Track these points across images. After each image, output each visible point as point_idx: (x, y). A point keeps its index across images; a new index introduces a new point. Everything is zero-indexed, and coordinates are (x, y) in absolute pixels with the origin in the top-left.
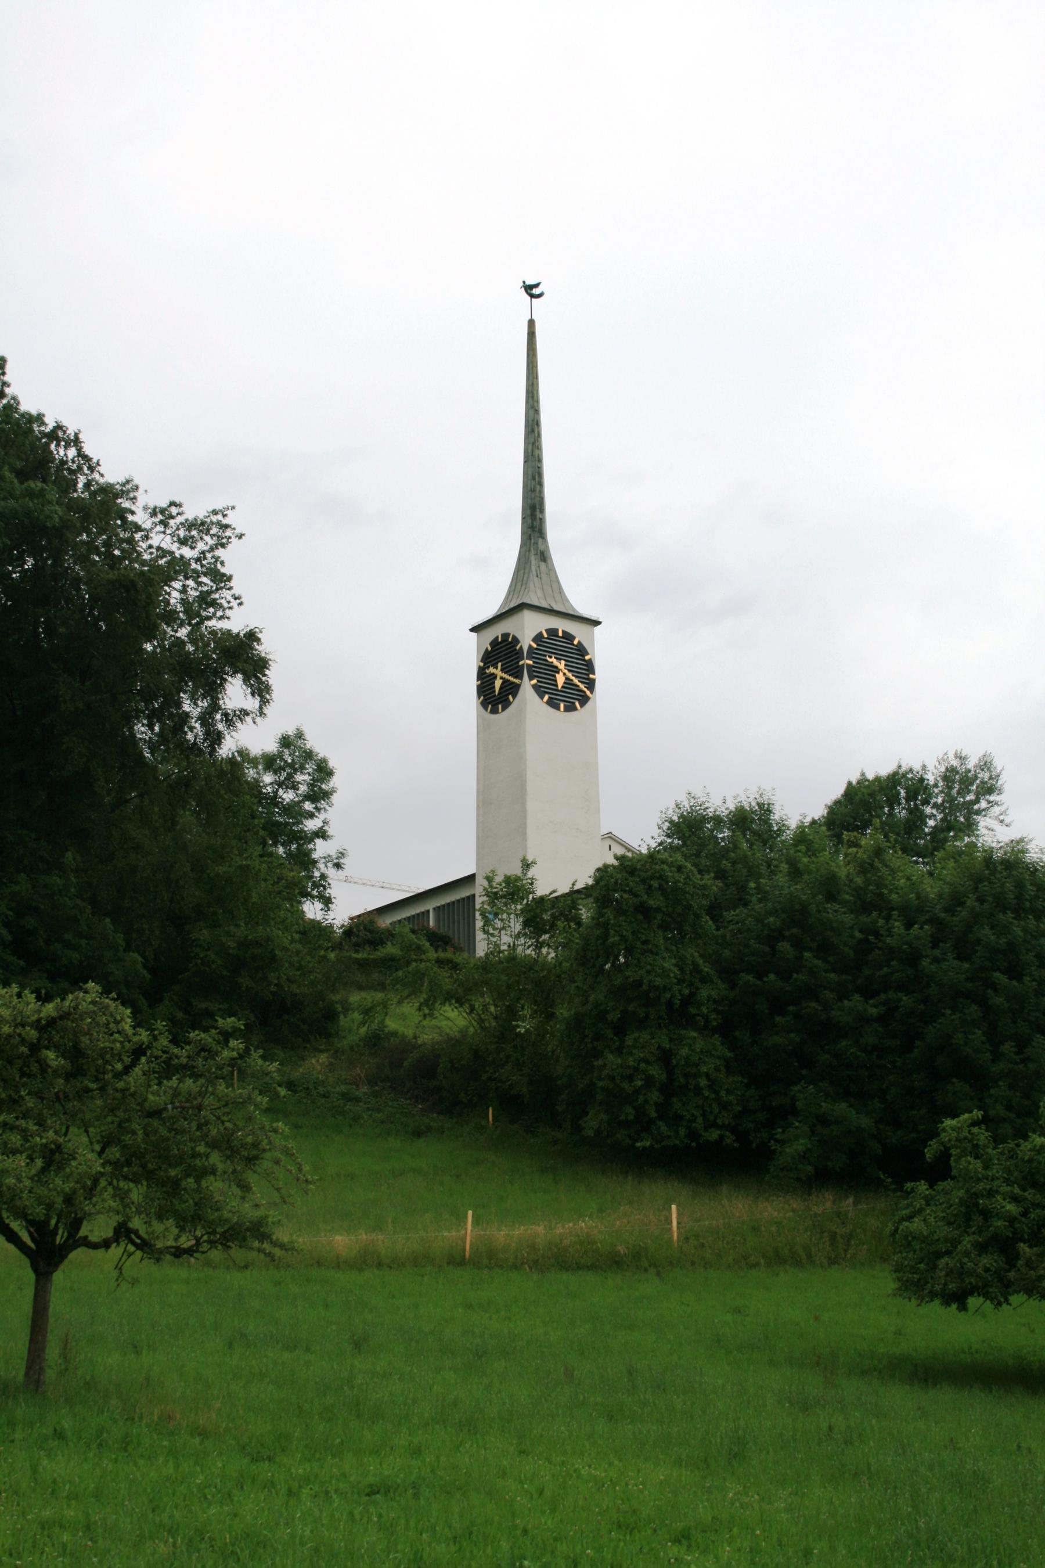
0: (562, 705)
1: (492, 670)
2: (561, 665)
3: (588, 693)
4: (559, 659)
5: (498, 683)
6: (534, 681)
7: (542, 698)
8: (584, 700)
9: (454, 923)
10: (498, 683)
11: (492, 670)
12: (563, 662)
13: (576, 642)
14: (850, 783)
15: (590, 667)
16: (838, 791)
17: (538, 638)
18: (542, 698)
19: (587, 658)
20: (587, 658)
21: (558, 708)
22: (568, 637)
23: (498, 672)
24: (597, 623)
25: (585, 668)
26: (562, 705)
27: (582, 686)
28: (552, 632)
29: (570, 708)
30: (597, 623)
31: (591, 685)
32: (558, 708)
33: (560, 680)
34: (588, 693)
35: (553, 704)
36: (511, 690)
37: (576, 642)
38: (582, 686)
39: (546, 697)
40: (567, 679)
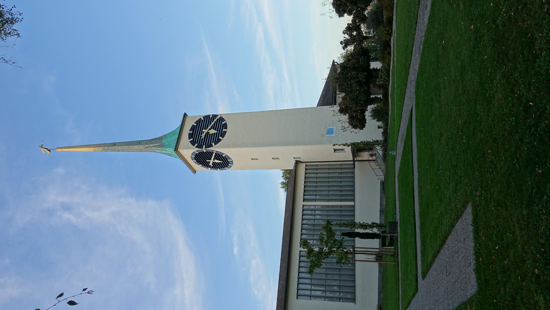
0: (224, 130)
1: (211, 164)
2: (205, 131)
3: (218, 118)
4: (202, 133)
5: (216, 161)
6: (213, 144)
7: (221, 140)
8: (222, 119)
9: (329, 186)
10: (216, 161)
11: (211, 164)
12: (203, 130)
13: (195, 125)
14: (283, 183)
15: (207, 117)
16: (326, 73)
17: (193, 143)
18: (221, 140)
19: (202, 119)
20: (202, 119)
21: (226, 132)
22: (193, 128)
23: (212, 161)
24: (185, 115)
25: (206, 121)
26: (224, 130)
27: (215, 120)
28: (190, 136)
29: (225, 126)
30: (185, 115)
31: (215, 116)
32: (226, 132)
33: (213, 131)
34: (218, 118)
35: (223, 134)
36: (219, 156)
37: (195, 125)
38: (215, 120)
39: (220, 138)
40: (211, 128)
